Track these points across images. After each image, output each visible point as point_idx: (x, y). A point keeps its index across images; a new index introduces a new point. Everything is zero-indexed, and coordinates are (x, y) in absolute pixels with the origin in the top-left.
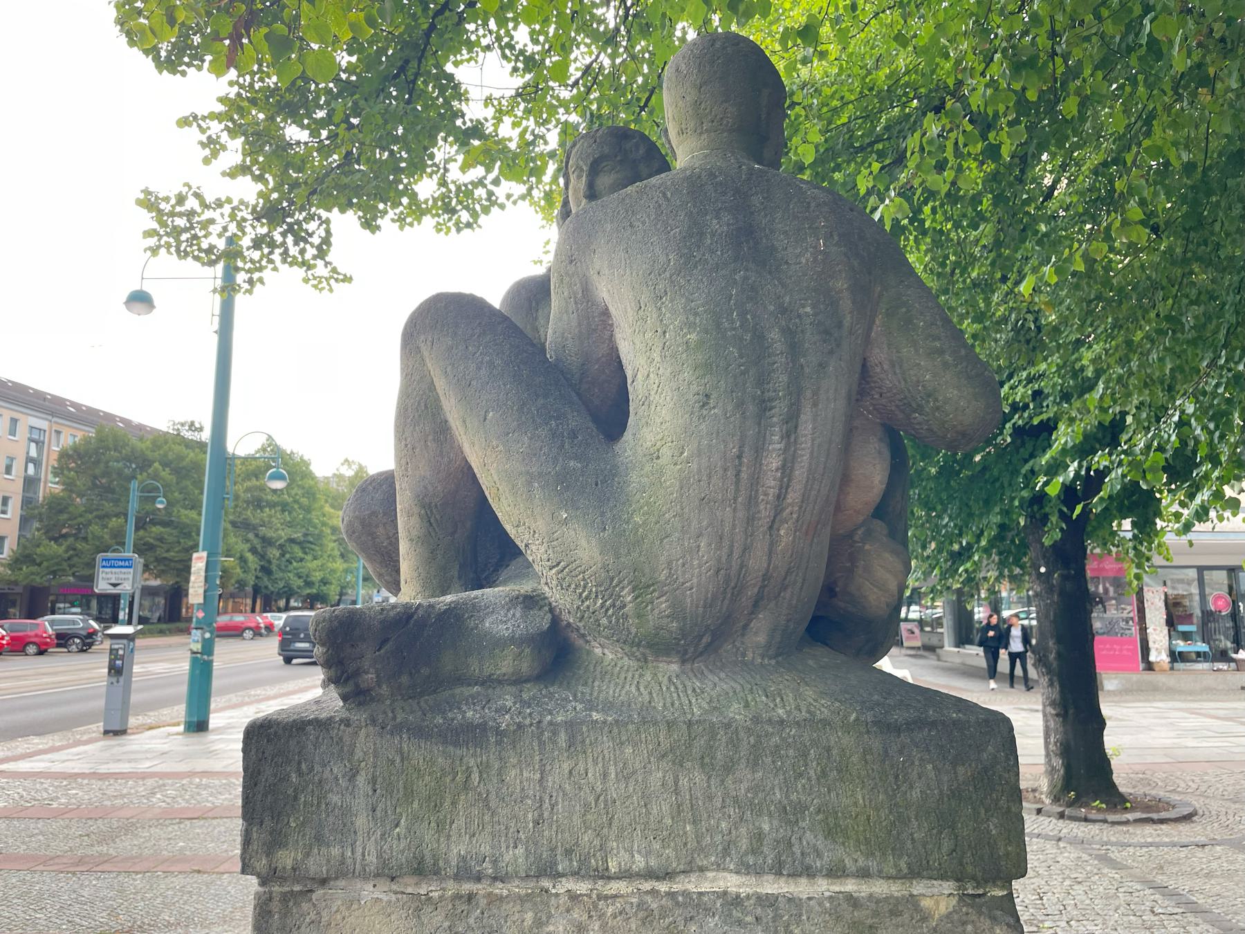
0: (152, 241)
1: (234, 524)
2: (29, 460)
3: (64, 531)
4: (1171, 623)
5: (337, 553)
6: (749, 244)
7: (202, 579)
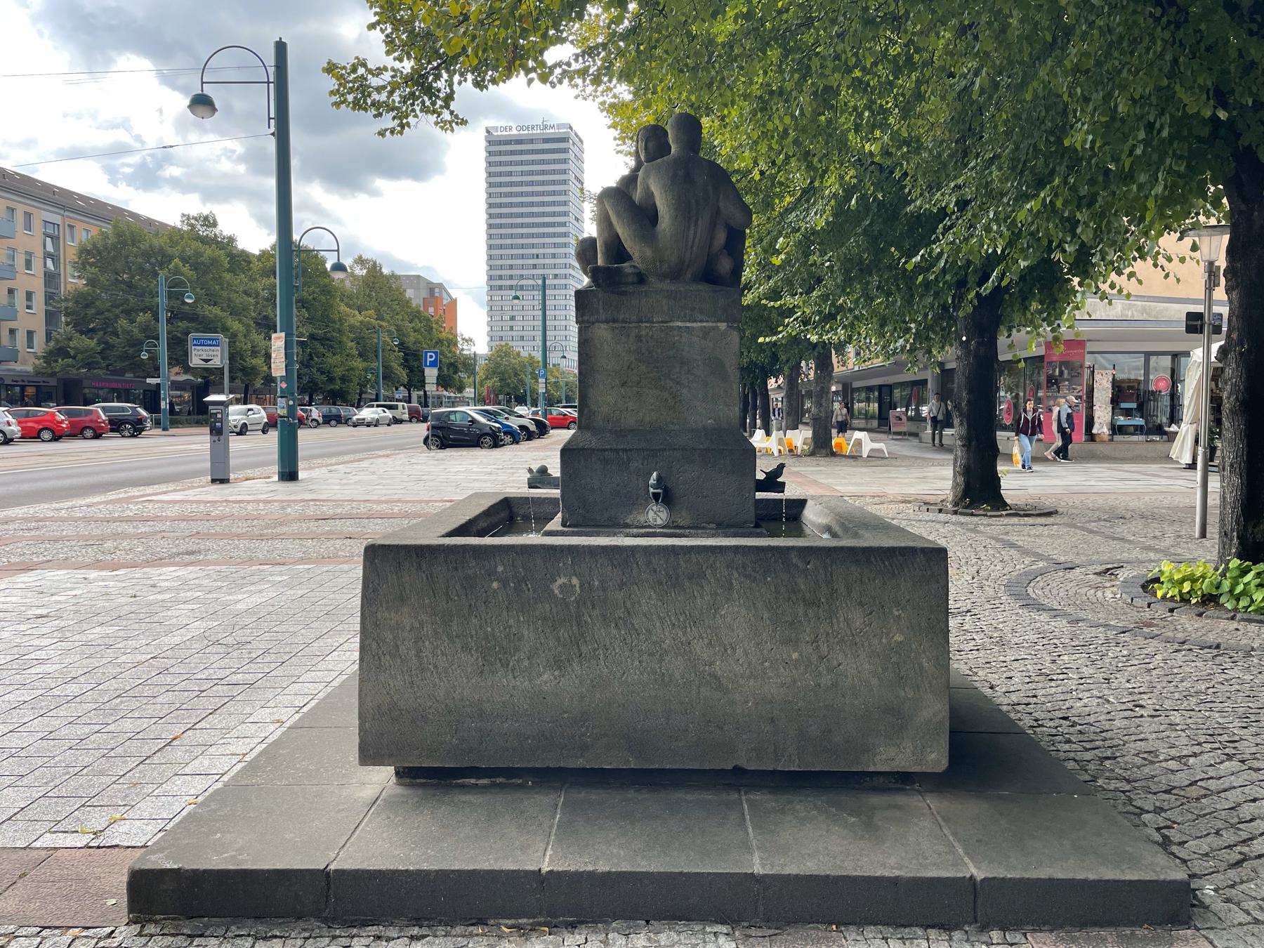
0: (336, 98)
2: (47, 255)
3: (92, 326)
4: (1115, 401)
5: (355, 352)
6: (688, 179)
7: (283, 355)
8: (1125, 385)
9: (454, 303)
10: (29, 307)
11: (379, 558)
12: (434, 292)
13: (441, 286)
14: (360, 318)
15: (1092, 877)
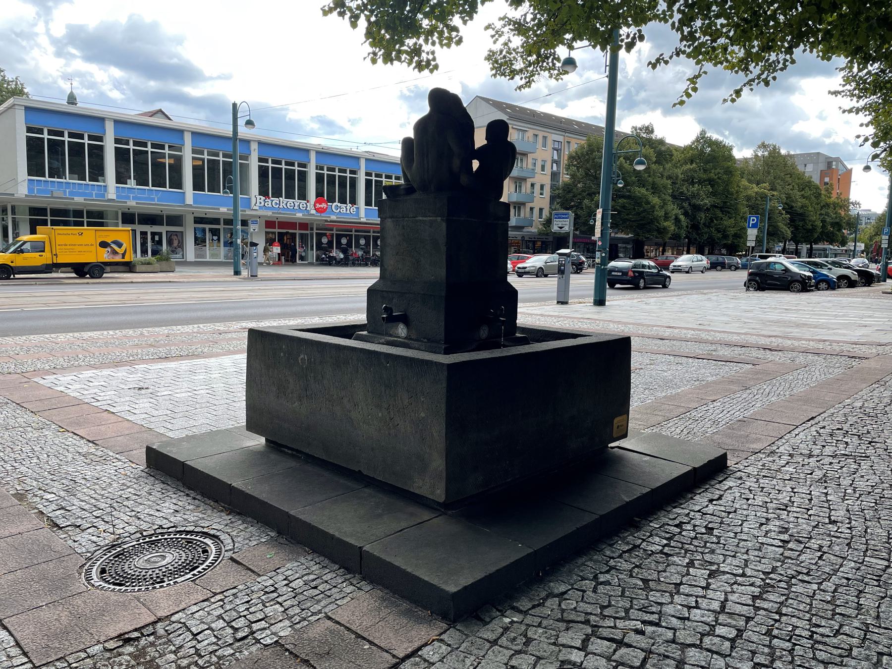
0: (494, 72)
1: (673, 196)
2: (554, 161)
8: (157, 266)
9: (849, 172)
10: (542, 194)
11: (255, 336)
13: (838, 160)
14: (756, 189)
15: (409, 570)
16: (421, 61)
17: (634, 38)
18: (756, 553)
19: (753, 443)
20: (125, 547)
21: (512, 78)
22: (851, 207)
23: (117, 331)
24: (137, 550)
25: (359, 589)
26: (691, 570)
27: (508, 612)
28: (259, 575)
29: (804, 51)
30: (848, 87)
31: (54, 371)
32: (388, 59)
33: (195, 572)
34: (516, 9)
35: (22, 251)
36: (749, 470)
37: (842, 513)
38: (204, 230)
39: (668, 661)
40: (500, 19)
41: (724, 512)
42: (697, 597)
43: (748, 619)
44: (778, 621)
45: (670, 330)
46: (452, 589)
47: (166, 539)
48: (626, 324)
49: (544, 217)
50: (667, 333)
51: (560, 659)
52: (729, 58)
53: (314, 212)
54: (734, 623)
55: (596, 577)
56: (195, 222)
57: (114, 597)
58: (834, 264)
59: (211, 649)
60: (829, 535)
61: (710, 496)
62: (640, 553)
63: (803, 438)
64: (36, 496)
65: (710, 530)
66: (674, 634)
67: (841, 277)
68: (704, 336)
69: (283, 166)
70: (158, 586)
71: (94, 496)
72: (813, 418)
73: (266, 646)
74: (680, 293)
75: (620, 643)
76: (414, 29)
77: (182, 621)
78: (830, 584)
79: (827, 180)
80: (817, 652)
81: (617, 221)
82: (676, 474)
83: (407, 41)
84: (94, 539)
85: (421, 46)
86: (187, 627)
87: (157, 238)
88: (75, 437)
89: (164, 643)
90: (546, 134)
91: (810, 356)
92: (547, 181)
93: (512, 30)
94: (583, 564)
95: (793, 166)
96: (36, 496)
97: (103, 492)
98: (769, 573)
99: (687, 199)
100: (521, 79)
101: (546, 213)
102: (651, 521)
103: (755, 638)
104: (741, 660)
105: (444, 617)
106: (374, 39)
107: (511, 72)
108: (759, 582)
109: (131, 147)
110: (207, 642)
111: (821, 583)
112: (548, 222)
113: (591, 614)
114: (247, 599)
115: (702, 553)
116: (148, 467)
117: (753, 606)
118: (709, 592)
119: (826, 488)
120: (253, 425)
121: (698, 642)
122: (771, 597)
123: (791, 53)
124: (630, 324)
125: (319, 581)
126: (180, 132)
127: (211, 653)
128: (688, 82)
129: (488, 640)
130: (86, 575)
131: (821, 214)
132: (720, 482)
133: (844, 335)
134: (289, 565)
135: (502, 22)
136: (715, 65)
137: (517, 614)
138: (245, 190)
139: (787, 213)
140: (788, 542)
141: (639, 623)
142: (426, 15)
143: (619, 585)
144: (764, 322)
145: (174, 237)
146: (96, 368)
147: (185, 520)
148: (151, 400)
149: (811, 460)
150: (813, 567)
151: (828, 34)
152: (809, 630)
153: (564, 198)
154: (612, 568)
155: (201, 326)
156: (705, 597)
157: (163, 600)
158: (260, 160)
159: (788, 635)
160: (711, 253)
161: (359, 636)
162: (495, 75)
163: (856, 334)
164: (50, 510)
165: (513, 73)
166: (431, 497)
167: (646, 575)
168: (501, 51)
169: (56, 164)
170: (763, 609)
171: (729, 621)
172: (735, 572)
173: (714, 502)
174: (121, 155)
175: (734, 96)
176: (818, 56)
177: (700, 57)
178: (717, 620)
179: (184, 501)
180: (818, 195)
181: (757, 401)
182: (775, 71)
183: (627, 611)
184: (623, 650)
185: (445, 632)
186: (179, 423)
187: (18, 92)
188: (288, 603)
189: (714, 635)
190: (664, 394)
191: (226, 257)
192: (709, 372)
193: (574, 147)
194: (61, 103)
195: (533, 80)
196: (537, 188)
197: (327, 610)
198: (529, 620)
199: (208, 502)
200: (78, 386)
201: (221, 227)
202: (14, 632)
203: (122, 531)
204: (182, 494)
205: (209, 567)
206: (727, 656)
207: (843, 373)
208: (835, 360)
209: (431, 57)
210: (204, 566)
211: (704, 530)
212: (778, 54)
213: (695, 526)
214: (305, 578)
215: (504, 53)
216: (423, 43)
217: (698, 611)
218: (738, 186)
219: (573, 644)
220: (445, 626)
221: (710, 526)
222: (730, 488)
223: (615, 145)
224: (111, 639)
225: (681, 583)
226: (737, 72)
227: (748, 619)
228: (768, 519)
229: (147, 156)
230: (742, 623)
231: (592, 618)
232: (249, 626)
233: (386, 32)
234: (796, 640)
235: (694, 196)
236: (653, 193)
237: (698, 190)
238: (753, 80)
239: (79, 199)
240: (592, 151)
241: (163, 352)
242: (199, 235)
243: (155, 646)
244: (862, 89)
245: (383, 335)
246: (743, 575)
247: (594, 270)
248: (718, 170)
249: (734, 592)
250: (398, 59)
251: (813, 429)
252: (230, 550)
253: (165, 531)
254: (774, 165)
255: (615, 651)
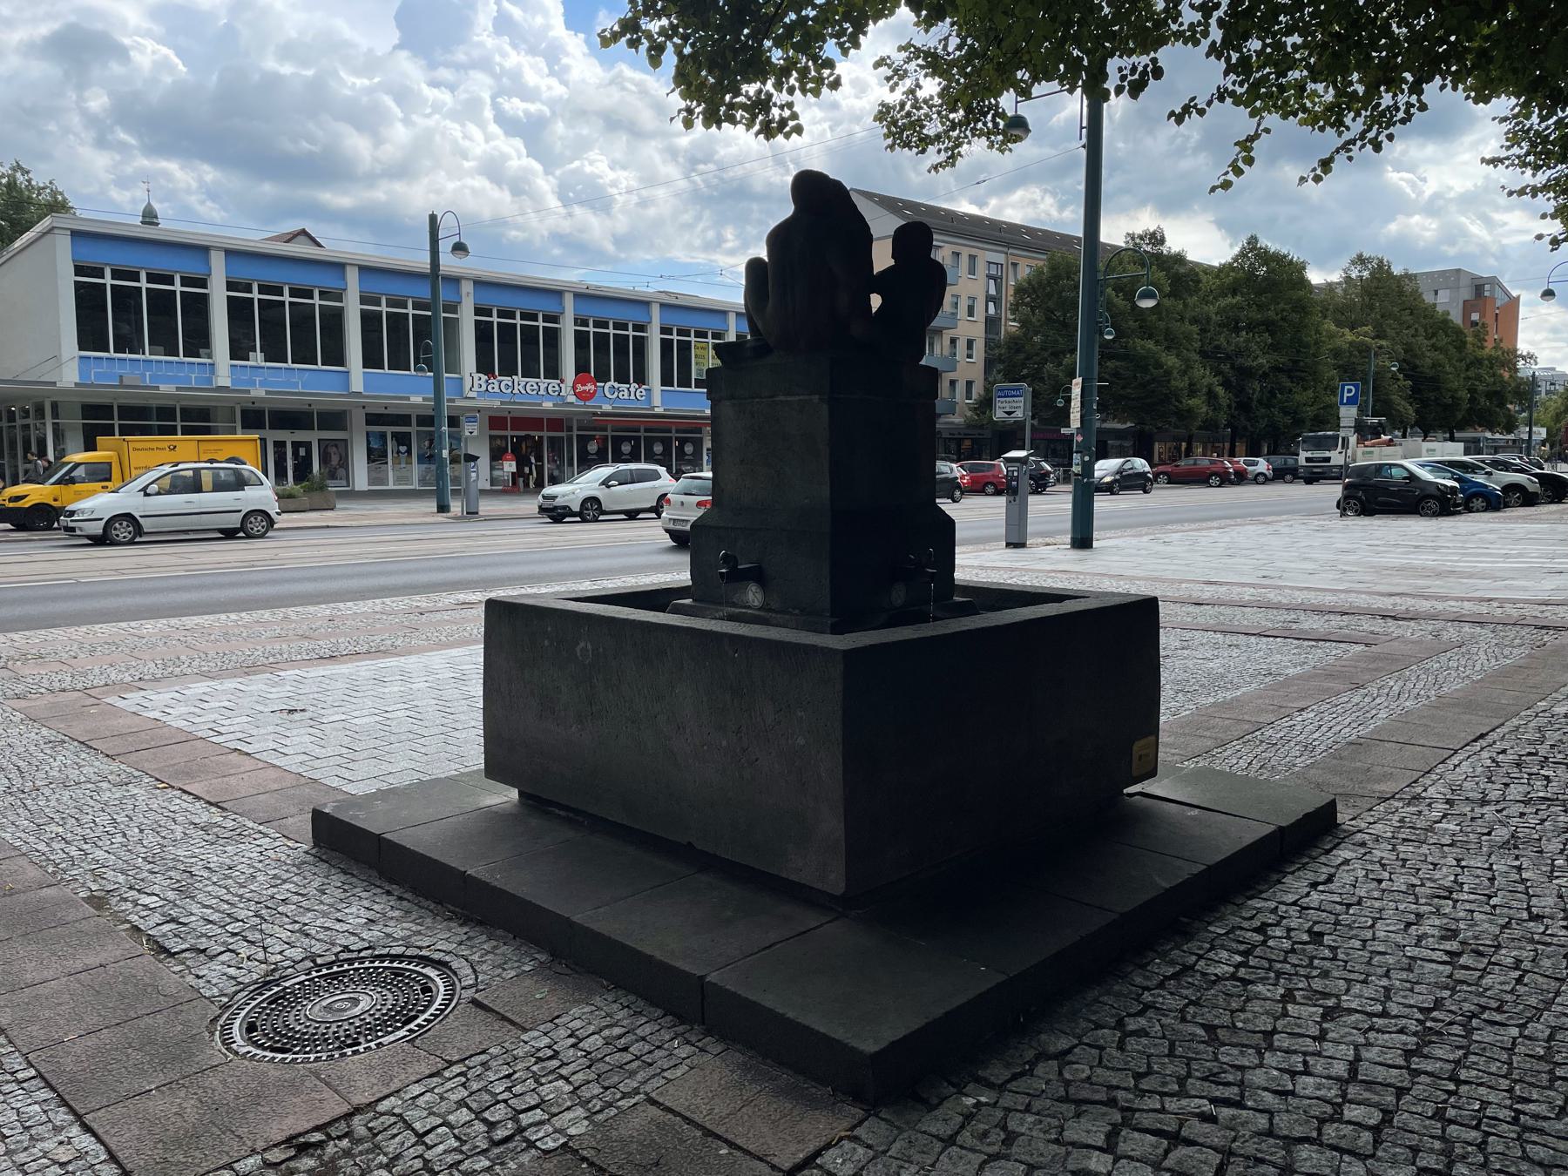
0: (890, 141)
1: (1202, 353)
2: (989, 298)
8: (305, 500)
9: (1514, 303)
10: (970, 356)
11: (497, 611)
12: (1481, 291)
13: (1494, 281)
14: (1350, 337)
15: (790, 1015)
16: (770, 122)
17: (1144, 73)
18: (1404, 975)
19: (1379, 781)
20: (287, 984)
21: (923, 151)
22: (1521, 364)
23: (243, 614)
24: (309, 990)
25: (701, 1050)
26: (1290, 1007)
27: (970, 1087)
28: (525, 1030)
29: (1443, 87)
30: (1516, 150)
31: (140, 684)
32: (712, 119)
33: (412, 1026)
34: (927, 31)
35: (73, 481)
36: (1378, 829)
37: (1550, 901)
38: (383, 436)
39: (1262, 1169)
40: (901, 49)
41: (1340, 903)
42: (1305, 1054)
43: (1401, 1092)
44: (1455, 1093)
45: (1212, 588)
46: (869, 1047)
47: (356, 970)
48: (1132, 579)
49: (975, 396)
50: (1207, 593)
51: (1070, 1167)
52: (1309, 105)
53: (572, 399)
54: (1376, 1098)
55: (1120, 1024)
56: (368, 423)
57: (273, 1073)
58: (1496, 464)
59: (450, 1159)
60: (1532, 941)
61: (1310, 876)
62: (1197, 979)
63: (1467, 769)
64: (126, 900)
65: (1317, 937)
66: (1271, 1120)
67: (1510, 488)
68: (1273, 596)
69: (518, 321)
70: (349, 1051)
71: (226, 897)
72: (1482, 736)
73: (546, 1152)
74: (1223, 523)
75: (1176, 1139)
76: (758, 68)
77: (396, 1111)
78: (1540, 1027)
79: (1475, 317)
80: (1529, 1147)
81: (1104, 401)
82: (1249, 838)
83: (745, 87)
84: (232, 971)
85: (770, 96)
86: (405, 1122)
87: (302, 452)
88: (185, 797)
89: (368, 1151)
90: (974, 252)
91: (1467, 628)
92: (977, 331)
93: (922, 67)
94: (1097, 1001)
95: (1416, 294)
96: (126, 900)
97: (241, 891)
98: (1430, 1010)
99: (1228, 357)
100: (939, 151)
101: (978, 390)
102: (1210, 924)
103: (1415, 1124)
104: (1394, 1162)
105: (857, 1097)
106: (689, 85)
107: (921, 140)
108: (1413, 1026)
109: (256, 295)
110: (442, 1147)
111: (1523, 1026)
112: (986, 403)
113: (1118, 1087)
114: (506, 1071)
115: (1307, 977)
116: (316, 845)
117: (1408, 1068)
118: (1326, 1045)
119: (1517, 858)
120: (496, 769)
121: (1315, 1134)
122: (1439, 1053)
123: (1420, 92)
124: (1139, 579)
125: (630, 1037)
126: (339, 267)
127: (451, 1166)
128: (1238, 149)
129: (937, 1137)
130: (222, 1034)
131: (1468, 378)
132: (1328, 852)
133: (1525, 589)
134: (575, 1011)
135: (904, 55)
136: (1285, 117)
137: (987, 1091)
138: (454, 366)
139: (1407, 377)
140: (1459, 955)
141: (1206, 1102)
142: (778, 43)
143: (1164, 1037)
144: (1380, 570)
145: (332, 450)
146: (213, 678)
147: (388, 935)
148: (312, 731)
149: (1485, 809)
150: (1508, 997)
151: (1483, 56)
152: (1511, 1108)
153: (1007, 360)
154: (1148, 1006)
155: (387, 601)
156: (1319, 1054)
157: (361, 1075)
158: (478, 311)
159: (1473, 1118)
160: (1273, 452)
161: (708, 1133)
162: (891, 147)
163: (1547, 587)
164: (151, 923)
165: (925, 142)
166: (819, 886)
167: (1209, 1017)
168: (902, 105)
169: (126, 329)
170: (1426, 1073)
171: (1367, 1095)
172: (1369, 1009)
173: (1321, 888)
174: (239, 310)
175: (1319, 172)
176: (1468, 98)
177: (1258, 104)
178: (1344, 1095)
179: (382, 905)
180: (1461, 345)
181: (1383, 705)
182: (1391, 123)
183: (1181, 1081)
184: (1182, 1151)
185: (860, 1123)
186: (363, 769)
187: (58, 206)
188: (578, 1079)
189: (1341, 1121)
190: (1211, 700)
191: (422, 481)
192: (1288, 660)
193: (1024, 271)
194: (131, 222)
195: (959, 154)
196: (961, 346)
197: (648, 1088)
198: (1007, 1100)
199: (426, 904)
200: (184, 710)
201: (413, 429)
202: (105, 1138)
203: (279, 957)
204: (379, 890)
205: (436, 1016)
206: (1368, 1157)
207: (1529, 656)
208: (1512, 633)
209: (787, 113)
210: (426, 1016)
211: (1306, 937)
212: (1395, 95)
213: (1289, 930)
214: (606, 1033)
215: (908, 107)
216: (772, 90)
217: (1309, 1080)
218: (1317, 332)
219: (1090, 1141)
220: (860, 1113)
221: (1316, 929)
222: (1346, 862)
223: (1101, 266)
224: (275, 1146)
225: (1274, 1031)
226: (1322, 129)
227: (1401, 1092)
228: (1419, 915)
229: (286, 311)
230: (1390, 1099)
231: (1120, 1094)
232: (515, 1119)
233: (710, 73)
234: (1488, 1125)
235: (1239, 353)
236: (1168, 348)
237: (1247, 341)
238: (1353, 142)
239: (165, 388)
240: (1058, 277)
241: (325, 647)
242: (374, 445)
243: (353, 1156)
244: (1541, 153)
245: (720, 604)
246: (1384, 1014)
247: (1070, 488)
248: (1282, 305)
249: (1371, 1045)
250: (732, 120)
251: (1485, 754)
252: (471, 986)
253: (354, 955)
254: (1383, 294)
255: (1167, 1152)
